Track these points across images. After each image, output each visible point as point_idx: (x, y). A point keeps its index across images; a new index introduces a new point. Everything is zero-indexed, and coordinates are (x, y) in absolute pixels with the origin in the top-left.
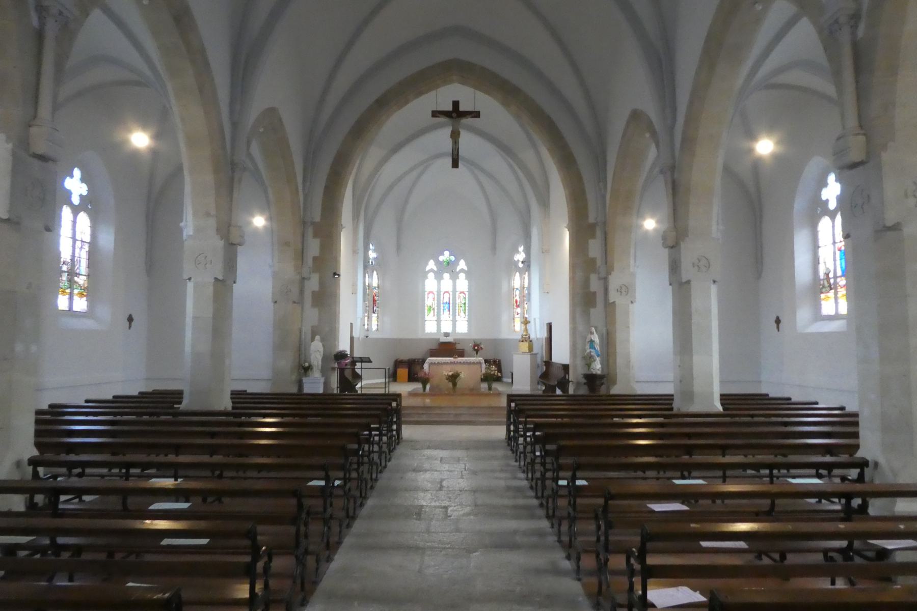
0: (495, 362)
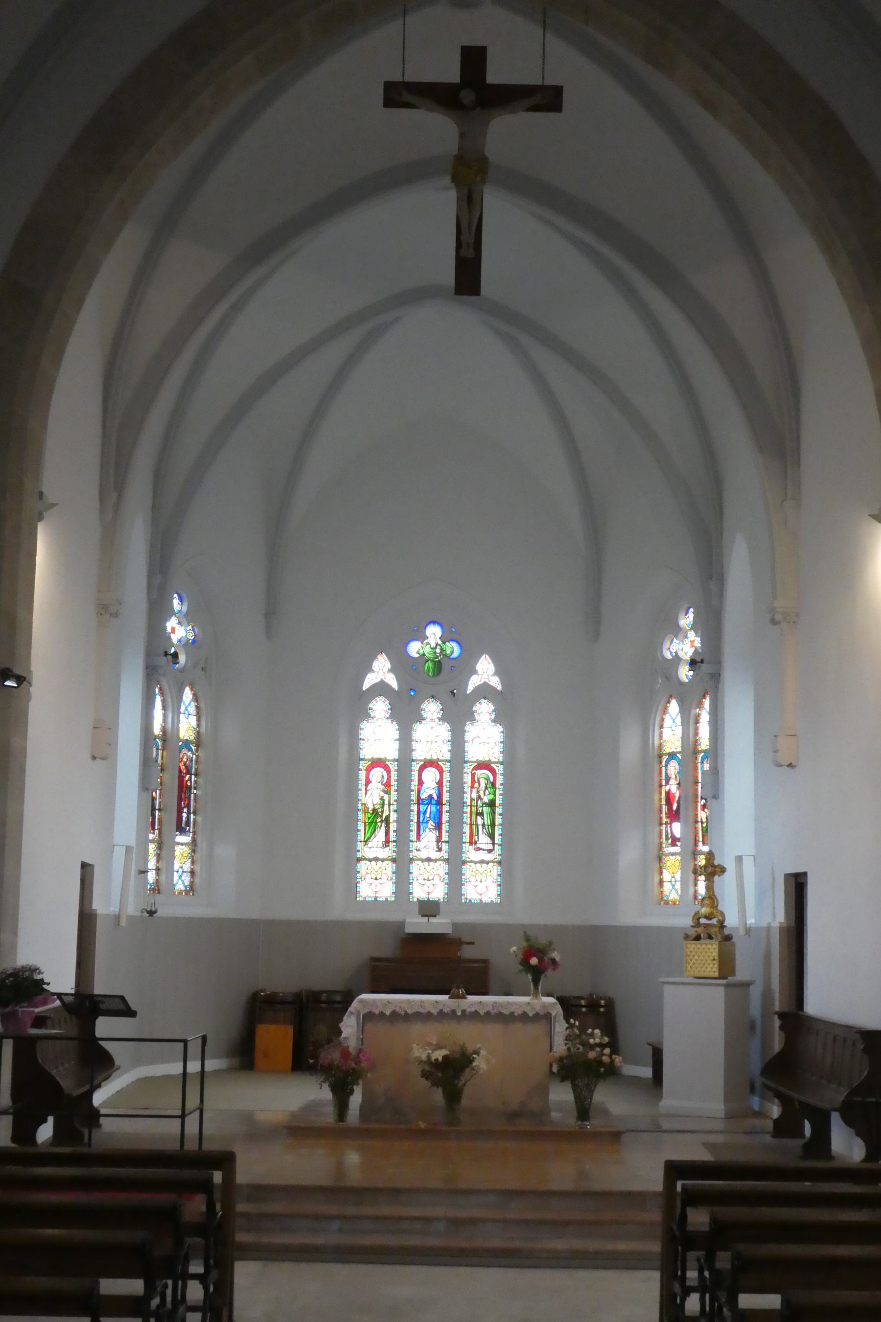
0: (593, 1005)
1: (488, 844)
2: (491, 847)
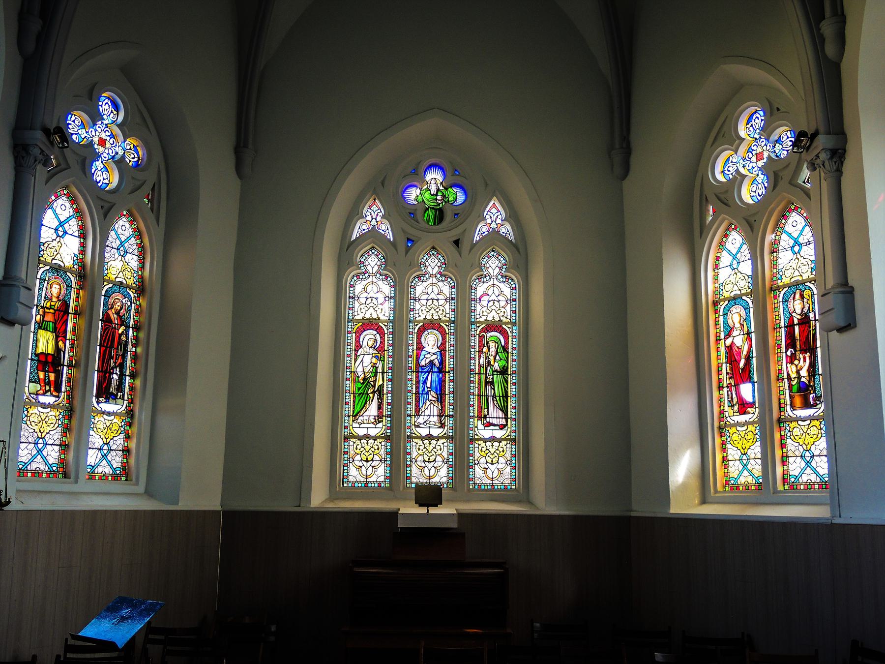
1: (499, 418)
2: (503, 422)
